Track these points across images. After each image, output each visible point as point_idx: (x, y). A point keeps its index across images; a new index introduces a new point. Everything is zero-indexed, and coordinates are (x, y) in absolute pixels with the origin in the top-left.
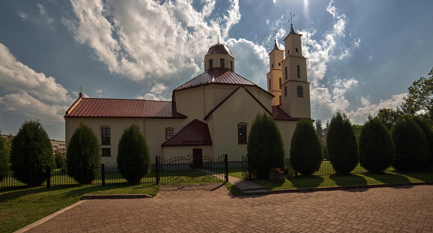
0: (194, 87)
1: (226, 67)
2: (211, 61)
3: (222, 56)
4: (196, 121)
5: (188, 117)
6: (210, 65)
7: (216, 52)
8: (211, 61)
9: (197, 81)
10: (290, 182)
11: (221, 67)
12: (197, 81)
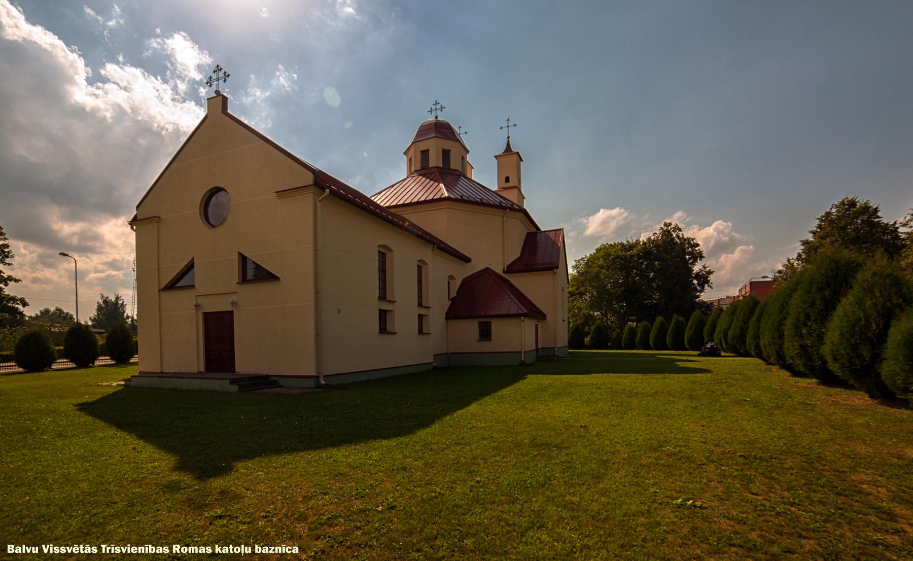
0: (469, 202)
1: (453, 166)
2: (425, 154)
3: (447, 144)
4: (487, 270)
5: (472, 260)
6: (449, 161)
7: (435, 137)
8: (425, 154)
9: (406, 197)
10: (838, 389)
11: (443, 165)
12: (406, 197)
